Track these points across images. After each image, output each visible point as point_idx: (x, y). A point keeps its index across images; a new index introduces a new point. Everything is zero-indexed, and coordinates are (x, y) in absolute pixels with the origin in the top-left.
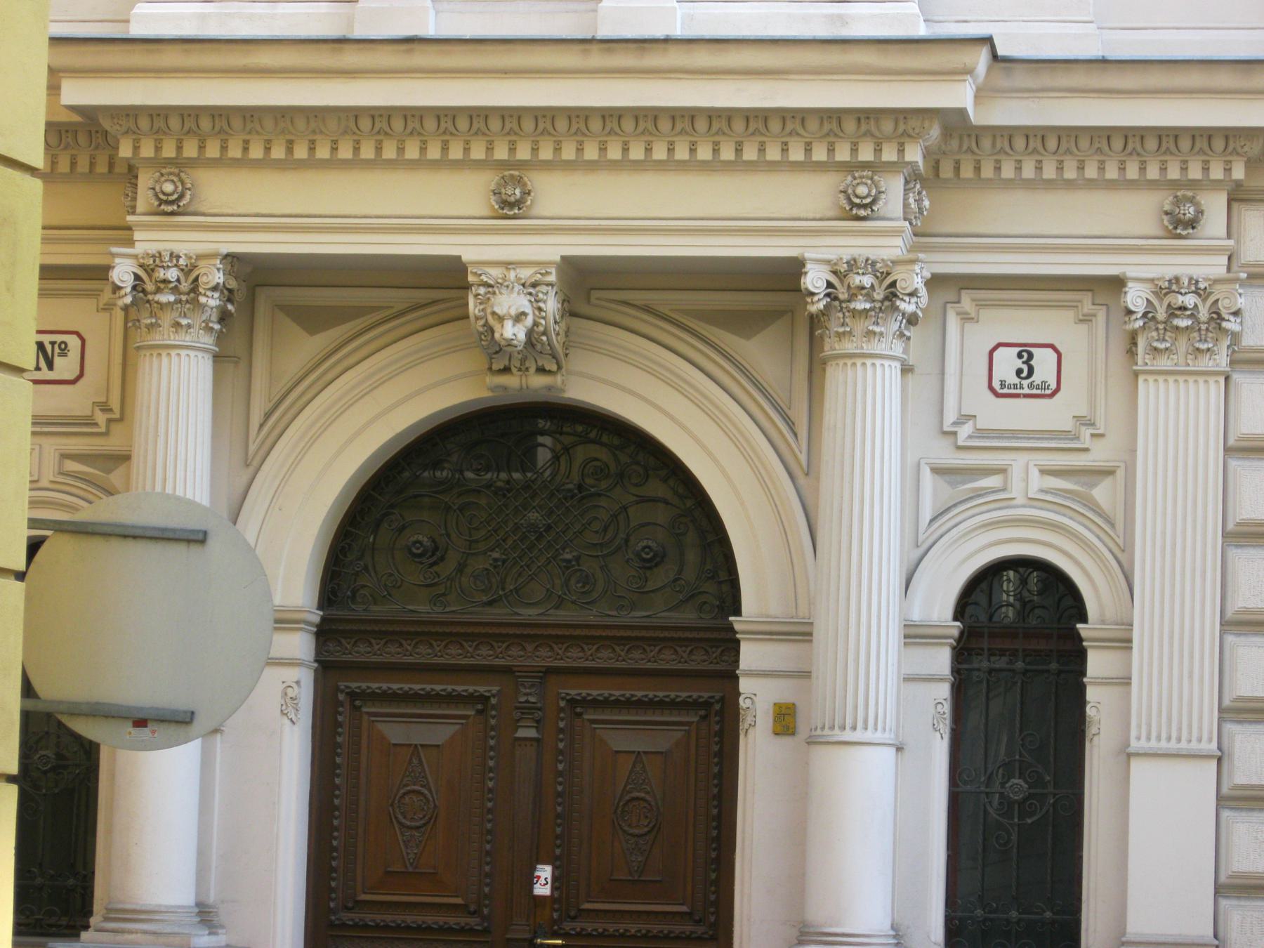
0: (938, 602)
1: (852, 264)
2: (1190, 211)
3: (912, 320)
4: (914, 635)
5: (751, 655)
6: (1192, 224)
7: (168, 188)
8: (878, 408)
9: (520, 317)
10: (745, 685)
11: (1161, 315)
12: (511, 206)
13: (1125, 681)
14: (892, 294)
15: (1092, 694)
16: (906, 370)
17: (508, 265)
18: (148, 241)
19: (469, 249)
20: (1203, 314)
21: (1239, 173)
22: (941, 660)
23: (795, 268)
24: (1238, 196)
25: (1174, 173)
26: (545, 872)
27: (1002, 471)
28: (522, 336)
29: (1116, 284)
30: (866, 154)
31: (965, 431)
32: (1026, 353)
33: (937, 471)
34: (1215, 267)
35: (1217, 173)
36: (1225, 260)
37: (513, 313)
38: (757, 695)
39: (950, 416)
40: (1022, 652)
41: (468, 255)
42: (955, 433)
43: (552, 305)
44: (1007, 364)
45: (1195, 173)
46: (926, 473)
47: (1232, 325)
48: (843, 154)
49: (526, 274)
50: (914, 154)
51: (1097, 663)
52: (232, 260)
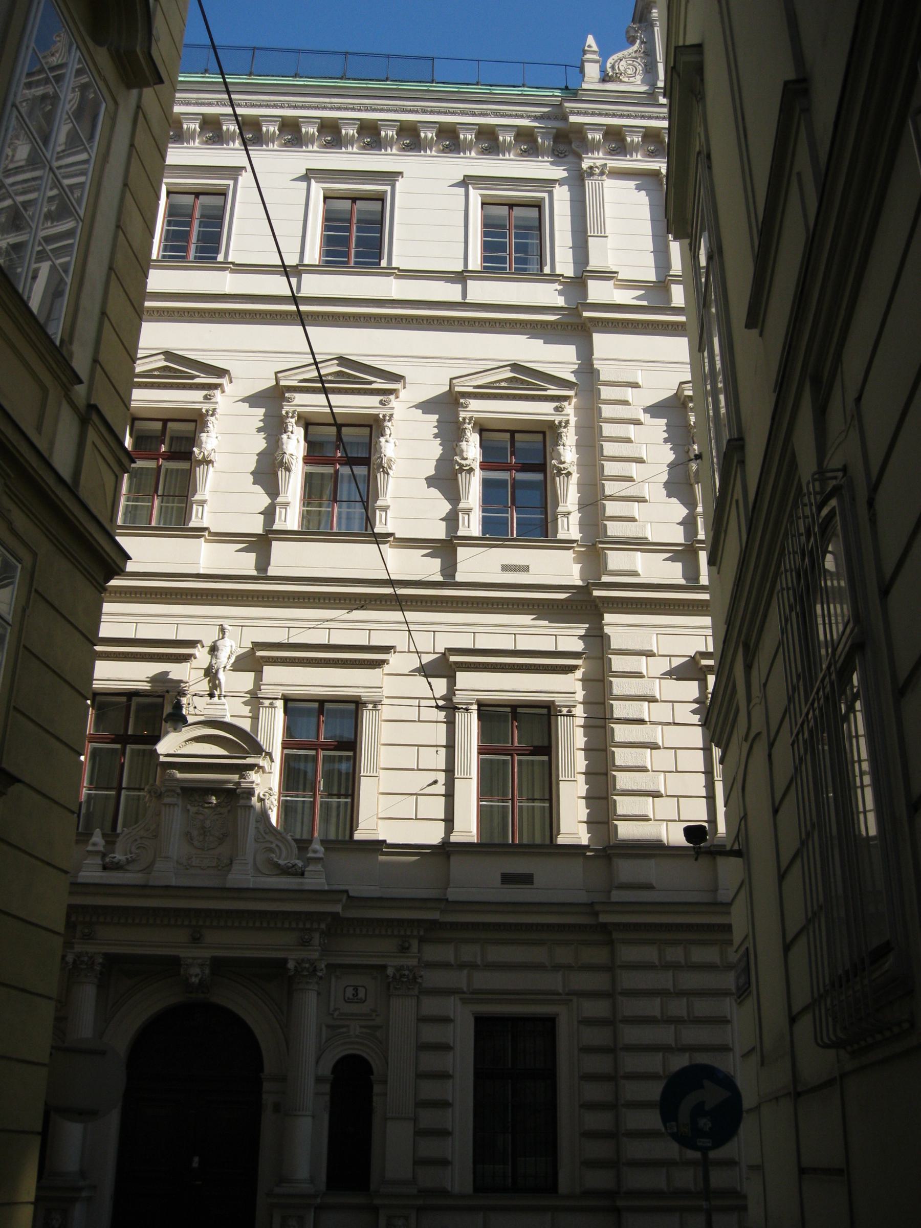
0: (326, 1068)
1: (303, 960)
2: (407, 945)
3: (321, 978)
4: (319, 1080)
5: (266, 1086)
6: (408, 948)
7: (86, 931)
8: (309, 1005)
9: (197, 975)
10: (264, 1096)
11: (398, 977)
12: (196, 940)
13: (385, 1094)
14: (315, 970)
15: (375, 1099)
16: (319, 994)
17: (194, 958)
18: (78, 948)
19: (182, 953)
20: (411, 977)
21: (422, 933)
22: (327, 1088)
23: (285, 961)
24: (422, 940)
25: (402, 933)
26: (196, 1159)
27: (348, 1026)
28: (197, 981)
29: (384, 967)
30: (308, 926)
31: (336, 1013)
32: (356, 989)
33: (328, 1026)
34: (413, 962)
35: (415, 933)
36: (417, 960)
37: (195, 974)
38: (268, 1099)
39: (332, 1008)
40: (353, 1085)
41: (182, 955)
42: (332, 1014)
43: (207, 971)
44: (350, 992)
45: (409, 933)
46: (324, 1028)
47: (419, 980)
48: (301, 926)
49: (199, 961)
50: (323, 926)
51: (377, 1089)
52: (106, 955)
